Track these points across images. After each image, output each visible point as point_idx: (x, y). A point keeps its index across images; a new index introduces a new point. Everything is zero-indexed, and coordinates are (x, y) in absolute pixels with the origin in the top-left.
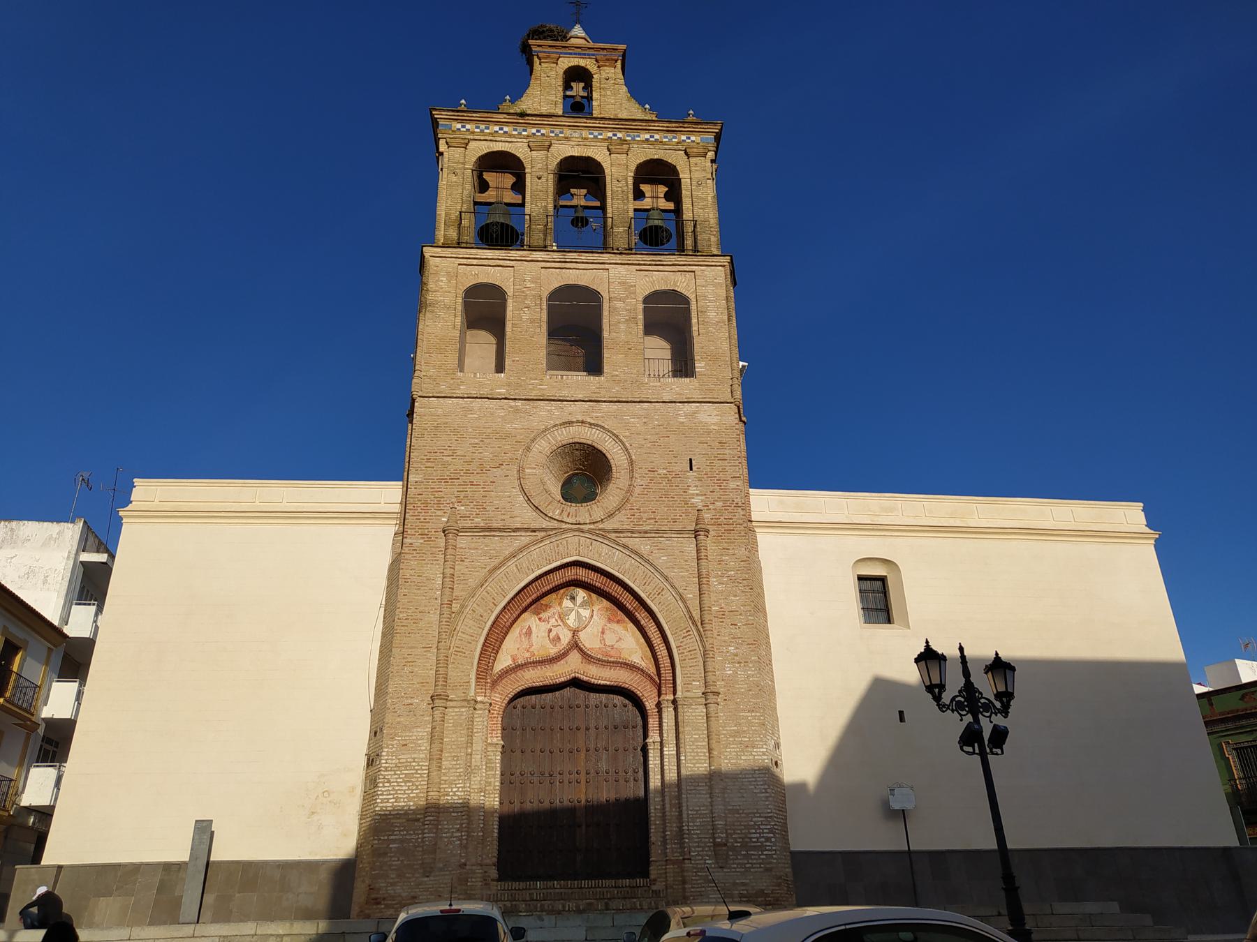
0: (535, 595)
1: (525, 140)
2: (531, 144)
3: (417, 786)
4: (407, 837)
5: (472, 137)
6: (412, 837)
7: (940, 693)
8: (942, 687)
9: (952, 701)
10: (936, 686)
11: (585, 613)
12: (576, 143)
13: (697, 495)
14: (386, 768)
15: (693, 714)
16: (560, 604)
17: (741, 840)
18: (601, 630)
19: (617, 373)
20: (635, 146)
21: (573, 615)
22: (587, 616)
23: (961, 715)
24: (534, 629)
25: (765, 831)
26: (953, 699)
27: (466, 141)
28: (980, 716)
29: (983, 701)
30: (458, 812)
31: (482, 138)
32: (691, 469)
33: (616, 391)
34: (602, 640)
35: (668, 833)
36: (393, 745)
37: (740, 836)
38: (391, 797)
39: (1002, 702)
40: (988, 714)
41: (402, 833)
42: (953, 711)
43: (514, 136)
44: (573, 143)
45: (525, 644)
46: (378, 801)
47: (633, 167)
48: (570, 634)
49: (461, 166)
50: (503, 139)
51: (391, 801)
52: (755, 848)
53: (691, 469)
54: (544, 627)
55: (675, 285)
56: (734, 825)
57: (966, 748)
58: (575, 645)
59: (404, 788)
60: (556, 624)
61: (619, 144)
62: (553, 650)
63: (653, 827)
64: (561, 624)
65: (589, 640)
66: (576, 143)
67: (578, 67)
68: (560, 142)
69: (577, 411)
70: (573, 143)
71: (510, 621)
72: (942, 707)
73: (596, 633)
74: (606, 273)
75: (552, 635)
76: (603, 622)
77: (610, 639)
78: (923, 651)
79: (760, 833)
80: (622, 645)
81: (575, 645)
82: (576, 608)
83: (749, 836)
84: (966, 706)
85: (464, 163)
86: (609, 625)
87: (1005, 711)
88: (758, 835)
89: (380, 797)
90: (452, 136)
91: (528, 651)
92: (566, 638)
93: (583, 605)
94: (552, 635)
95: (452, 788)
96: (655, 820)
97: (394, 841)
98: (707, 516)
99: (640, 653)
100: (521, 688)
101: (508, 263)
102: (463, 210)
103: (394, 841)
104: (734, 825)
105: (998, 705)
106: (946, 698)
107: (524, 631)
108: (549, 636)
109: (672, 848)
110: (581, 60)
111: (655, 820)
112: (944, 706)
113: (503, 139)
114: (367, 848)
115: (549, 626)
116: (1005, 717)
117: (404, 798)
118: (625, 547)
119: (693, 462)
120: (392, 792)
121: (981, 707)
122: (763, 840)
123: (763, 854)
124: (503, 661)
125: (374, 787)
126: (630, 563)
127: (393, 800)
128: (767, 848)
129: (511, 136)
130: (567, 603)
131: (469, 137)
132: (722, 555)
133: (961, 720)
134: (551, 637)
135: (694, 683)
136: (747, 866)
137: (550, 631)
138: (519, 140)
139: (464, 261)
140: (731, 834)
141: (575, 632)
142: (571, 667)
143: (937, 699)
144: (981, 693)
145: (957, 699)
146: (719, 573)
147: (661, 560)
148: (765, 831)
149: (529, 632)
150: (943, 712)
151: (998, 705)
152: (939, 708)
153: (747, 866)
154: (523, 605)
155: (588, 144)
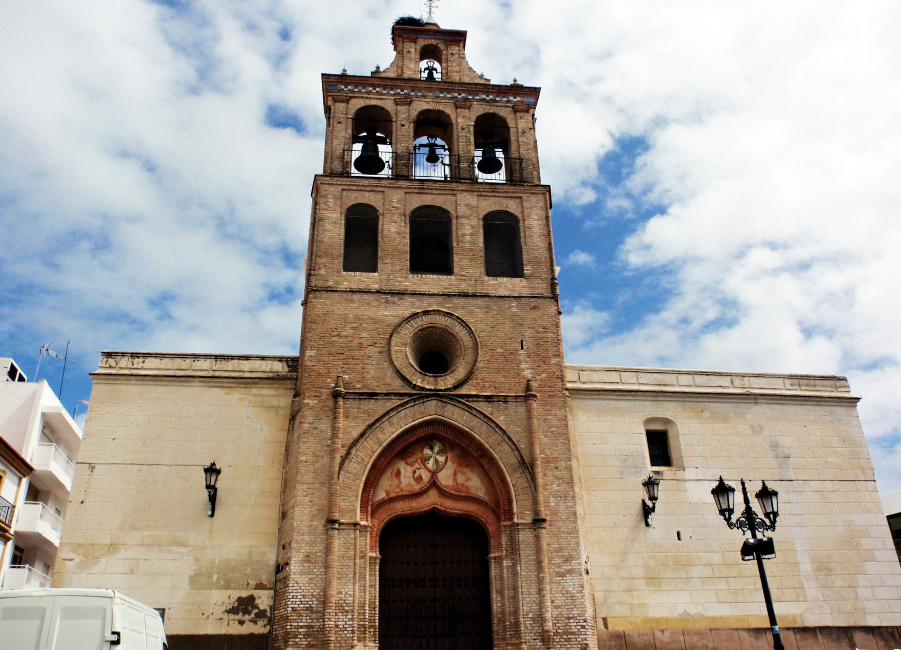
0: (403, 445)
1: (392, 98)
2: (397, 100)
3: (318, 587)
4: (312, 624)
5: (352, 95)
6: (316, 624)
7: (730, 516)
8: (731, 511)
9: (737, 522)
10: (726, 510)
11: (441, 459)
12: (431, 100)
13: (527, 369)
14: (294, 573)
15: (526, 536)
16: (422, 452)
17: (563, 628)
18: (453, 472)
19: (464, 273)
20: (475, 103)
21: (431, 461)
22: (443, 462)
23: (743, 531)
24: (402, 470)
25: (581, 621)
26: (738, 520)
27: (349, 98)
28: (756, 531)
29: (758, 520)
30: (349, 607)
31: (360, 96)
32: (522, 348)
33: (464, 287)
34: (455, 479)
35: (508, 623)
36: (299, 555)
37: (563, 625)
38: (299, 594)
39: (770, 519)
40: (761, 530)
41: (308, 621)
42: (738, 528)
43: (384, 95)
44: (428, 100)
45: (396, 482)
46: (289, 597)
47: (474, 118)
48: (429, 475)
49: (344, 116)
50: (376, 96)
51: (298, 597)
52: (572, 633)
53: (522, 348)
54: (410, 469)
55: (507, 207)
56: (558, 617)
57: (746, 558)
58: (433, 484)
59: (308, 588)
60: (419, 467)
61: (463, 101)
62: (417, 487)
63: (496, 619)
64: (423, 467)
65: (445, 478)
66: (431, 100)
67: (432, 45)
68: (419, 99)
69: (433, 304)
70: (428, 100)
71: (385, 464)
72: (730, 525)
73: (450, 474)
74: (454, 197)
75: (416, 475)
76: (455, 466)
77: (461, 479)
78: (761, 489)
79: (577, 623)
80: (470, 484)
81: (433, 484)
82: (434, 455)
83: (569, 624)
84: (747, 524)
85: (346, 114)
86: (459, 468)
87: (773, 526)
88: (576, 624)
89: (291, 594)
90: (337, 94)
91: (398, 487)
92: (426, 476)
93: (438, 453)
94: (416, 475)
95: (344, 589)
96: (497, 615)
97: (302, 627)
98: (534, 384)
99: (483, 490)
100: (393, 515)
101: (380, 189)
102: (346, 149)
103: (302, 627)
104: (558, 617)
105: (767, 521)
106: (734, 519)
107: (395, 472)
108: (414, 476)
109: (511, 634)
110: (433, 41)
111: (497, 615)
112: (732, 524)
113: (376, 96)
114: (281, 631)
115: (414, 468)
116: (773, 531)
117: (308, 596)
118: (472, 408)
119: (524, 343)
120: (299, 591)
121: (747, 524)
122: (579, 627)
123: (579, 638)
124: (381, 495)
125: (286, 587)
126: (476, 422)
127: (301, 597)
128: (583, 633)
129: (382, 94)
130: (427, 451)
131: (350, 95)
132: (547, 415)
133: (744, 534)
134: (415, 477)
135: (526, 512)
136: (568, 646)
137: (414, 472)
138: (388, 97)
139: (347, 187)
140: (555, 624)
141: (434, 473)
142: (431, 500)
143: (728, 520)
144: (757, 515)
145: (741, 520)
146: (545, 429)
147: (500, 419)
148: (581, 621)
149: (398, 474)
150: (732, 529)
151: (767, 521)
152: (729, 526)
153: (568, 646)
154: (394, 452)
155: (439, 100)
